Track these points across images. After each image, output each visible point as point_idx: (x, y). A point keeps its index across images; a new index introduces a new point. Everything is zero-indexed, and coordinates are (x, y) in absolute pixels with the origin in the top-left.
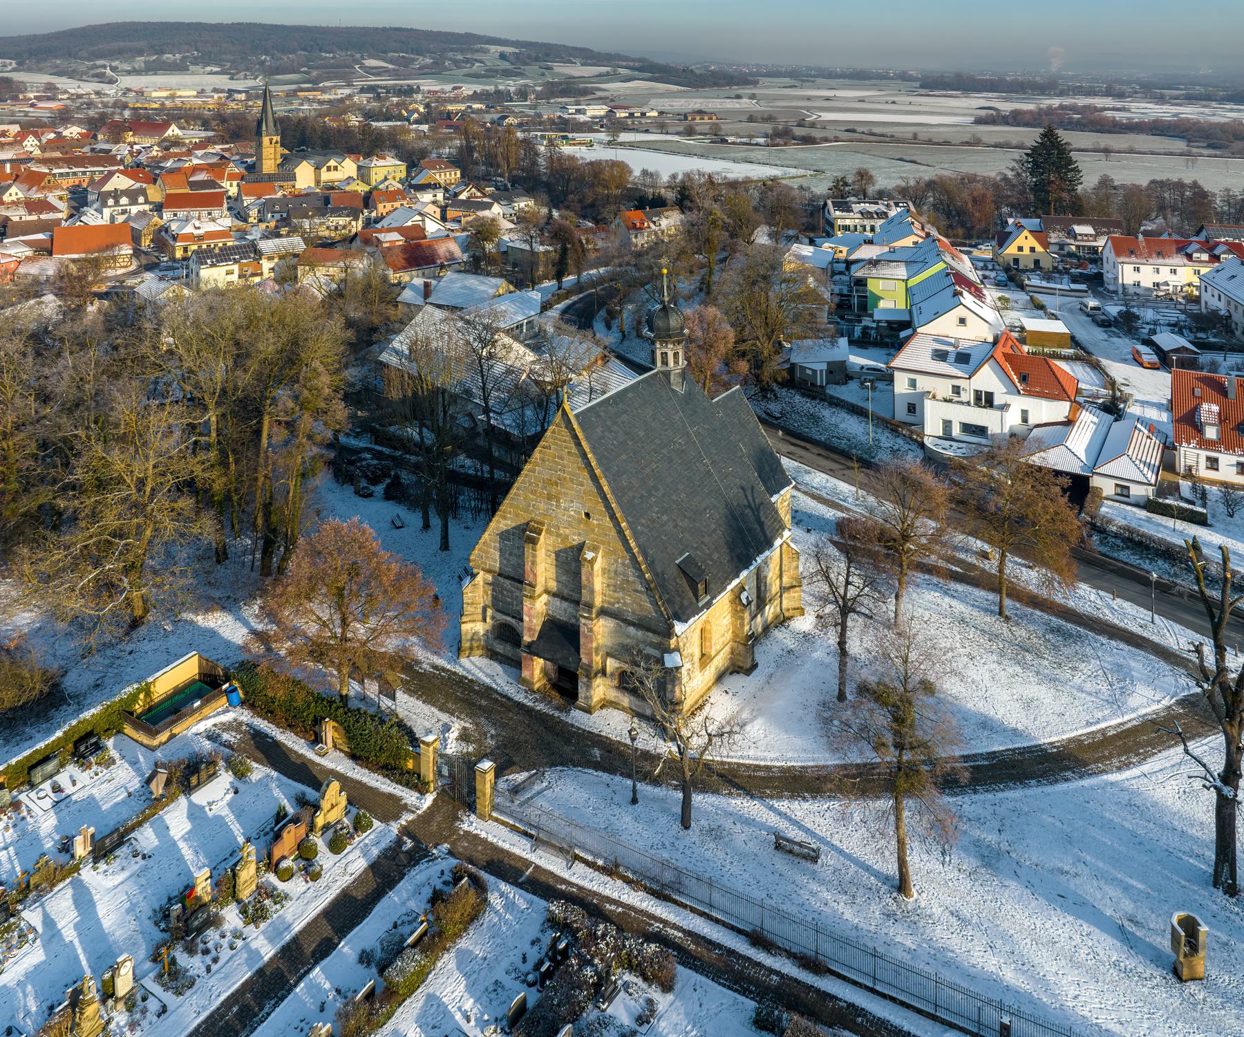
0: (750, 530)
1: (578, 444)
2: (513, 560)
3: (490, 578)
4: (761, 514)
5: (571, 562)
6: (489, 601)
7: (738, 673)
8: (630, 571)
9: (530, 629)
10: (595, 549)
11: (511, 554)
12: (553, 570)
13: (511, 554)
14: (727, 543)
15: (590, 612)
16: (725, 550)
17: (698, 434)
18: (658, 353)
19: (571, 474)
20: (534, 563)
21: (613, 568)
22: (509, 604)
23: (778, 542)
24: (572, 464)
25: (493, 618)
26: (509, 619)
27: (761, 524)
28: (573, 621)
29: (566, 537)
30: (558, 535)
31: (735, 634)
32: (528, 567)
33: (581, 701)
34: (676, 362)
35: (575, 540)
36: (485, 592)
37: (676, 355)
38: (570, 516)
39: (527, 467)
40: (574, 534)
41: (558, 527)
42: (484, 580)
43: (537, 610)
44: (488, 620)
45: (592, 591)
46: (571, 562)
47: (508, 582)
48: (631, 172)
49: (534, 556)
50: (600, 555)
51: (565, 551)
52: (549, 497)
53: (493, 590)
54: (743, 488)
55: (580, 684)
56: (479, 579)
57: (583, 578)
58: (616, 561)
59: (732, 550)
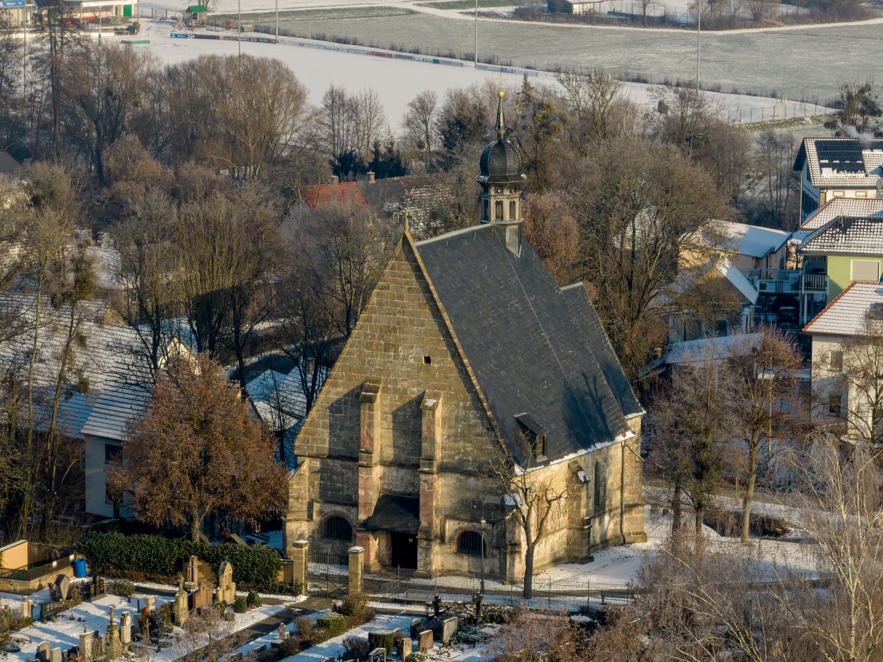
0: (590, 417)
1: (420, 276)
2: (345, 435)
3: (317, 464)
4: (604, 405)
5: (411, 420)
6: (316, 493)
7: (573, 563)
8: (471, 414)
9: (366, 504)
10: (436, 396)
11: (342, 429)
12: (390, 434)
13: (342, 429)
14: (565, 419)
15: (430, 465)
16: (562, 424)
17: (535, 305)
18: (493, 202)
19: (412, 314)
20: (371, 425)
21: (454, 414)
22: (339, 490)
23: (620, 438)
24: (414, 302)
25: (320, 512)
26: (339, 508)
27: (603, 417)
28: (411, 489)
29: (405, 391)
30: (396, 391)
31: (571, 520)
32: (364, 433)
33: (420, 569)
34: (512, 215)
35: (414, 392)
36: (311, 484)
37: (512, 204)
38: (409, 365)
39: (363, 316)
40: (413, 386)
41: (395, 382)
42: (310, 468)
43: (374, 481)
44: (315, 517)
45: (433, 441)
46: (411, 420)
47: (338, 463)
48: (297, 96)
49: (371, 417)
50: (440, 401)
51: (402, 409)
52: (387, 348)
53: (322, 478)
54: (584, 375)
55: (419, 550)
56: (305, 468)
57: (424, 428)
58: (457, 406)
59: (570, 427)
